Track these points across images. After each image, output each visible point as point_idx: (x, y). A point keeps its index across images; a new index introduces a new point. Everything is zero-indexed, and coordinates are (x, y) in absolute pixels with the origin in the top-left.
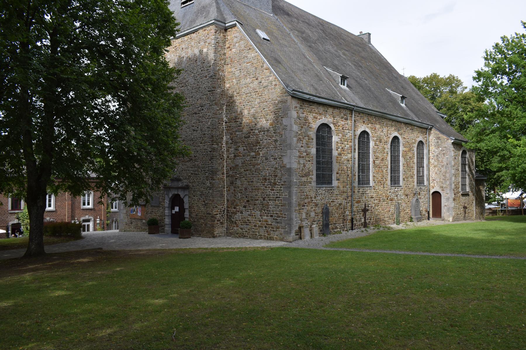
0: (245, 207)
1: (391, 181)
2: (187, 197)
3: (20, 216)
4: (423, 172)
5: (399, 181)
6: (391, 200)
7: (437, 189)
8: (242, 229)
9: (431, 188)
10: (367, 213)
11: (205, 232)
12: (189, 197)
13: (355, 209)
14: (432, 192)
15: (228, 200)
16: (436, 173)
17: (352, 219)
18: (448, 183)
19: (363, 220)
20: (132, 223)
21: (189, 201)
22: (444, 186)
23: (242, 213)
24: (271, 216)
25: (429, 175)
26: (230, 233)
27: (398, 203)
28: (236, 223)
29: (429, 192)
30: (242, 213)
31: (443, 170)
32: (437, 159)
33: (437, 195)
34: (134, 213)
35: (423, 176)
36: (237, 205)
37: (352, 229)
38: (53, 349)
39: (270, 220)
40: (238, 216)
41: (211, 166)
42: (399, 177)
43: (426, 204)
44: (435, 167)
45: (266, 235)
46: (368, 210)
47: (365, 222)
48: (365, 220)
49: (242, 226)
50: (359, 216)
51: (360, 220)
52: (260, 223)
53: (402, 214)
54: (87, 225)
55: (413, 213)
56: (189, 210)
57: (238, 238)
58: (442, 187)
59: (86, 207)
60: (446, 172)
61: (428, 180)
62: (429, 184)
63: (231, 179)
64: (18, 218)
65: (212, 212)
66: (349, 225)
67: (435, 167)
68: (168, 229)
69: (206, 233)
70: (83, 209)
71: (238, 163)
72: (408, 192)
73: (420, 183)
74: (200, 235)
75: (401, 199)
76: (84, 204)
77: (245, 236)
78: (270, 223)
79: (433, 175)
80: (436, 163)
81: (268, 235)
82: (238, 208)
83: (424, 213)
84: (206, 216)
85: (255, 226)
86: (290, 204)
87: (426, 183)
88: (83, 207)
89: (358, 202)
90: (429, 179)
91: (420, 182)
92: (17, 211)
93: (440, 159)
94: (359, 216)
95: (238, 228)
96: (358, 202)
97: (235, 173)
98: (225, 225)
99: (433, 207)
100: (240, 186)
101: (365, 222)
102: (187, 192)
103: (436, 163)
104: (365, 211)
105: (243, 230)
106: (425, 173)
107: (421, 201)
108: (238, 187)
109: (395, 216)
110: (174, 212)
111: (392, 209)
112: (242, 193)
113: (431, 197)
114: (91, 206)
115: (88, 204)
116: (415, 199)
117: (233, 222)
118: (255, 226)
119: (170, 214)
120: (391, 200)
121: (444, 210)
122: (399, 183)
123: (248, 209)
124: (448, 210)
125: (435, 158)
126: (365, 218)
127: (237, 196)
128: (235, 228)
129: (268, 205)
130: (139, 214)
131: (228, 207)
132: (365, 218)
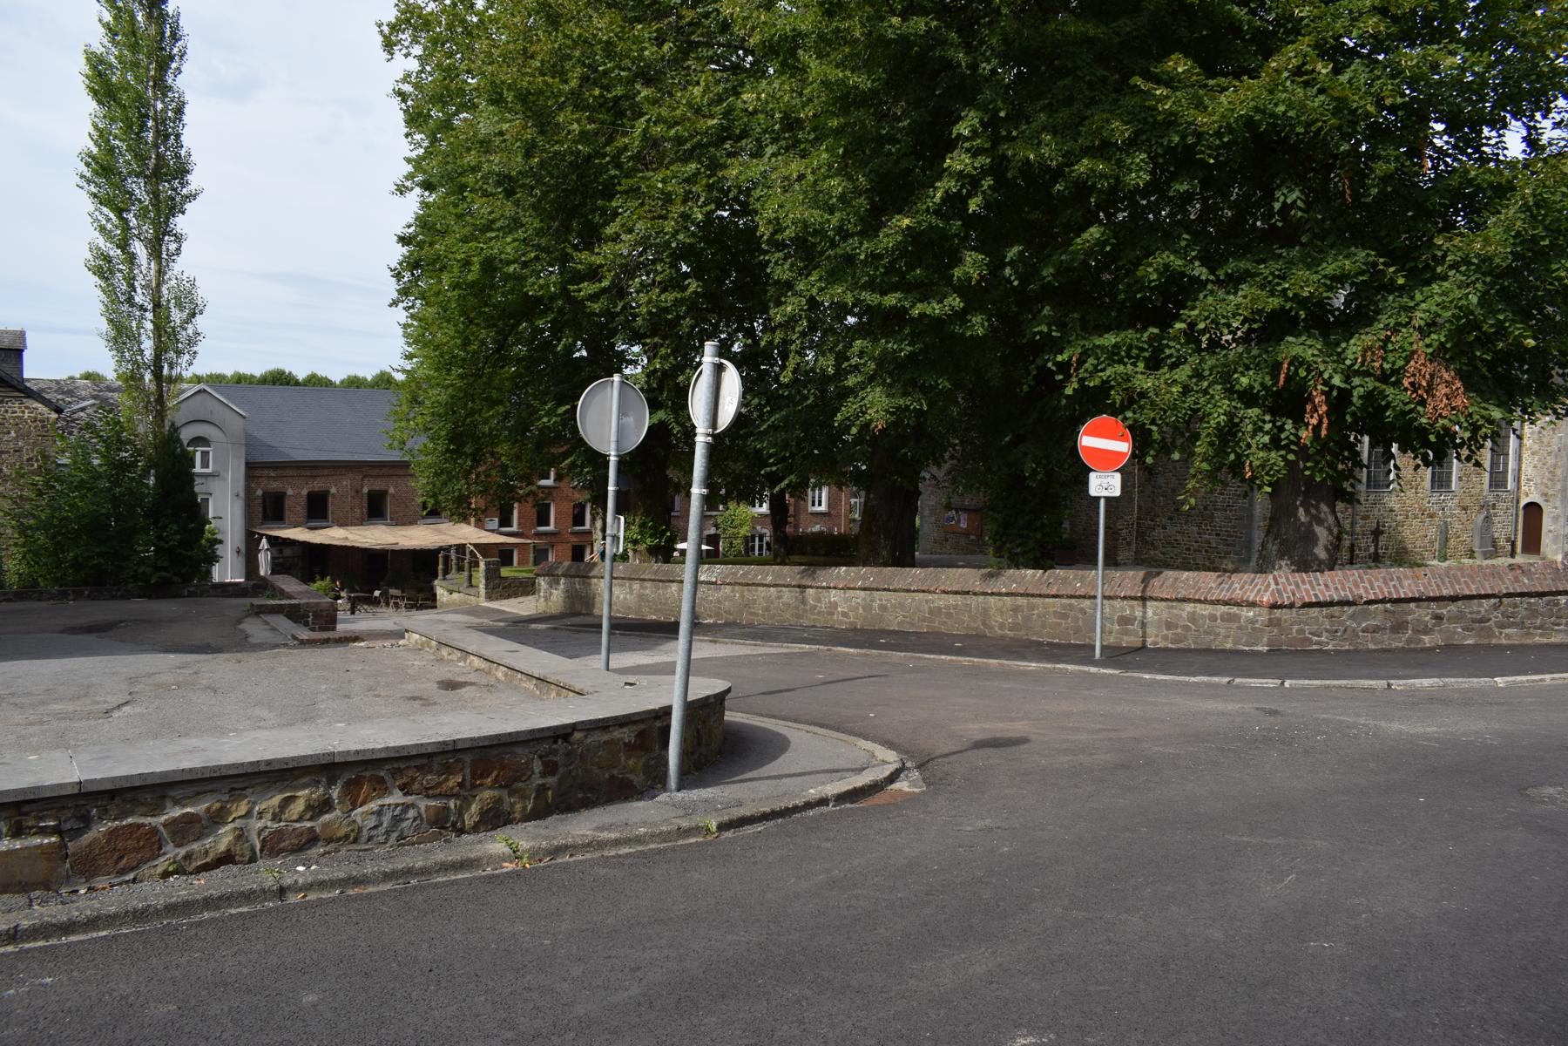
0: (1171, 519)
1: (1433, 481)
3: (719, 521)
4: (1506, 464)
5: (1450, 482)
6: (1431, 516)
7: (1534, 497)
8: (1163, 553)
9: (1522, 496)
10: (1381, 538)
13: (1358, 529)
14: (1523, 502)
15: (1140, 508)
16: (1535, 467)
17: (1352, 546)
18: (1559, 486)
19: (1372, 549)
20: (947, 540)
22: (1550, 492)
23: (1164, 528)
24: (1217, 535)
25: (1520, 469)
27: (1446, 523)
29: (1518, 502)
30: (1164, 528)
31: (1550, 460)
32: (1540, 439)
33: (1533, 510)
35: (1505, 472)
36: (1157, 516)
37: (1352, 563)
38: (1565, 459)
39: (1214, 541)
40: (1158, 533)
42: (1451, 473)
43: (1507, 525)
44: (1533, 454)
45: (1207, 564)
46: (1383, 532)
47: (1376, 553)
48: (1376, 549)
50: (1365, 543)
51: (1367, 549)
52: (1196, 545)
53: (1452, 543)
54: (527, 563)
55: (1477, 541)
58: (1546, 495)
59: (817, 509)
60: (1555, 466)
61: (1518, 479)
62: (1519, 488)
64: (716, 526)
66: (1345, 555)
67: (1533, 454)
70: (812, 514)
72: (1467, 502)
73: (1497, 486)
75: (1452, 516)
76: (813, 505)
79: (1527, 470)
80: (1536, 447)
83: (1502, 543)
85: (1188, 549)
86: (1251, 517)
87: (1510, 485)
88: (812, 509)
89: (1365, 518)
90: (1519, 478)
91: (1498, 481)
92: (714, 513)
93: (1545, 440)
94: (1365, 543)
96: (1365, 518)
98: (1134, 547)
99: (1523, 533)
101: (1376, 553)
103: (1536, 447)
104: (1377, 533)
106: (1511, 465)
107: (1496, 519)
108: (1160, 487)
109: (1437, 545)
111: (1432, 532)
113: (1521, 513)
114: (823, 508)
115: (820, 504)
116: (1482, 517)
118: (1188, 549)
120: (1431, 516)
121: (1546, 540)
122: (1449, 486)
124: (1555, 539)
125: (1536, 436)
126: (1376, 546)
129: (1212, 517)
130: (963, 525)
131: (1139, 518)
132: (1376, 546)
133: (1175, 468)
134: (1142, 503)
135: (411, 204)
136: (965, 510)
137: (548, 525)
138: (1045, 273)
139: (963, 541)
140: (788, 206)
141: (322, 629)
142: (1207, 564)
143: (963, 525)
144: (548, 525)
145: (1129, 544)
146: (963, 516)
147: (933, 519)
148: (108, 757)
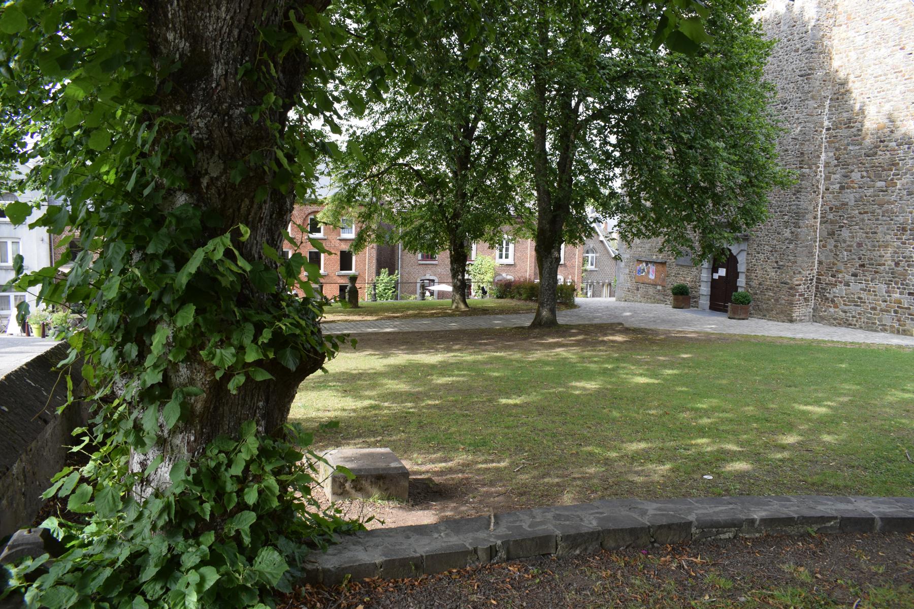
0: (855, 275)
2: (745, 253)
8: (845, 312)
11: (774, 312)
12: (748, 254)
15: (820, 263)
20: (638, 289)
21: (747, 260)
23: (847, 284)
26: (820, 317)
28: (833, 301)
30: (847, 284)
34: (644, 274)
40: (839, 290)
41: (797, 205)
45: (896, 325)
49: (846, 308)
52: (883, 305)
56: (746, 275)
57: (836, 326)
63: (830, 227)
65: (791, 280)
68: (705, 302)
69: (777, 313)
71: (847, 200)
74: (765, 316)
77: (850, 324)
78: (906, 306)
81: (899, 325)
82: (840, 276)
84: (778, 287)
85: (874, 309)
95: (837, 310)
97: (840, 216)
98: (812, 303)
100: (848, 239)
102: (744, 246)
105: (848, 314)
108: (845, 241)
110: (716, 276)
112: (851, 251)
115: (507, 257)
117: (827, 299)
118: (874, 309)
119: (710, 280)
123: (862, 280)
127: (841, 256)
128: (832, 310)
130: (652, 276)
131: (819, 274)
133: (863, 220)
134: (823, 259)
135: (873, 121)
136: (654, 263)
137: (351, 270)
138: (562, 39)
139: (651, 291)
140: (780, 53)
141: (9, 301)
142: (896, 325)
143: (652, 276)
144: (351, 270)
145: (806, 300)
146: (652, 268)
147: (627, 271)
148: (360, 543)
